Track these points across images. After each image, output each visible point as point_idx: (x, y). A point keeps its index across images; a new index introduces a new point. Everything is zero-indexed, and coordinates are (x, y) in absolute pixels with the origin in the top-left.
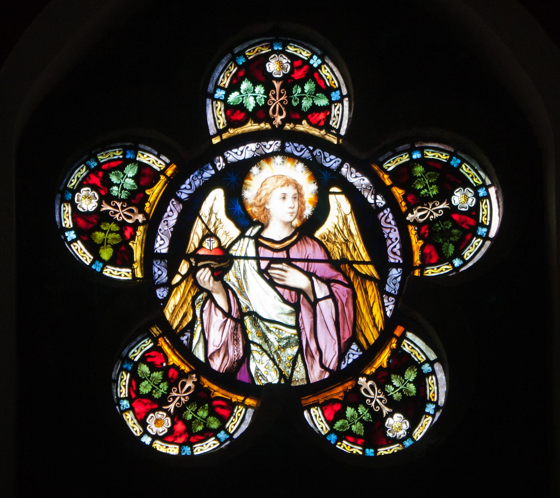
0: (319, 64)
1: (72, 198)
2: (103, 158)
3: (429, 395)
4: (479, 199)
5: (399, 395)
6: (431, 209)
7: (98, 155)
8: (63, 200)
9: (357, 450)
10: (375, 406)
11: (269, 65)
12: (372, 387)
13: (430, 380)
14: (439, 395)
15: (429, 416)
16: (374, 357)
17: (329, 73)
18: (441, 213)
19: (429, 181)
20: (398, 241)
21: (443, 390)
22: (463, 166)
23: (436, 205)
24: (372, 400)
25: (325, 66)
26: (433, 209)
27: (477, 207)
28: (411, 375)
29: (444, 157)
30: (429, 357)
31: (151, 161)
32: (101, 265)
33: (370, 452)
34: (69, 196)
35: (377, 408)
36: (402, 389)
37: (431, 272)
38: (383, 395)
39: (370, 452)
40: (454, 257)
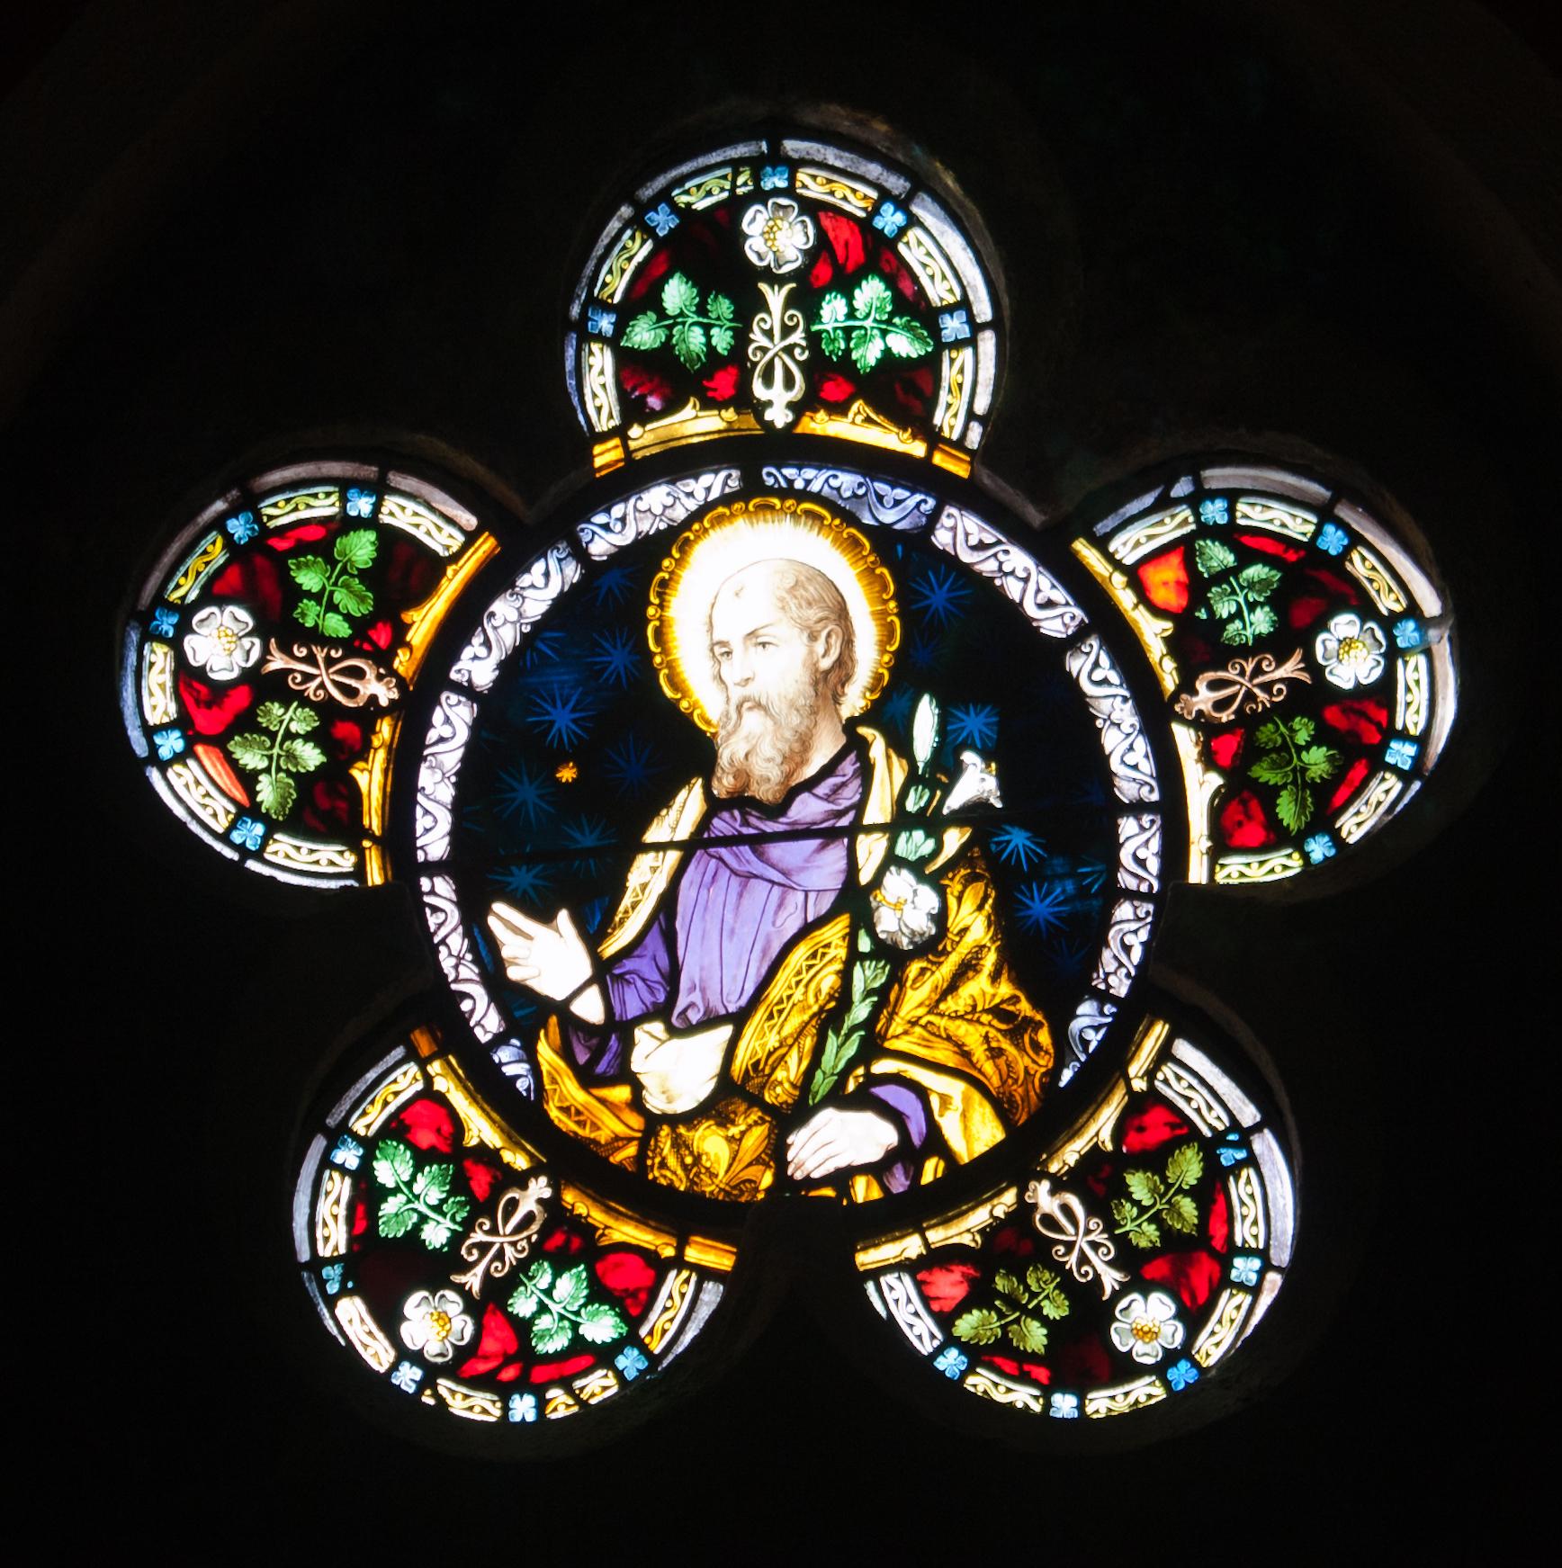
0: (959, 337)
1: (974, 846)
2: (279, 512)
3: (1243, 1233)
4: (1393, 654)
5: (1151, 1230)
6: (1251, 679)
7: (262, 505)
8: (150, 636)
9: (1023, 1396)
10: (1080, 1265)
11: (759, 211)
12: (1214, 685)
13: (1242, 1189)
14: (980, 366)
15: (1239, 1291)
16: (1077, 1119)
17: (1254, 1200)
18: (1280, 691)
19: (1246, 597)
20: (1155, 828)
21: (1285, 1224)
22: (1355, 556)
23: (1266, 669)
24: (1070, 1246)
25: (1252, 1172)
26: (1256, 681)
27: (1388, 680)
28: (1189, 1167)
29: (1298, 525)
30: (1239, 1117)
31: (421, 528)
32: (259, 829)
33: (1064, 1405)
34: (167, 624)
35: (1083, 1272)
36: (1160, 1211)
37: (1239, 869)
38: (1102, 1232)
39: (1064, 1405)
40: (1310, 831)
